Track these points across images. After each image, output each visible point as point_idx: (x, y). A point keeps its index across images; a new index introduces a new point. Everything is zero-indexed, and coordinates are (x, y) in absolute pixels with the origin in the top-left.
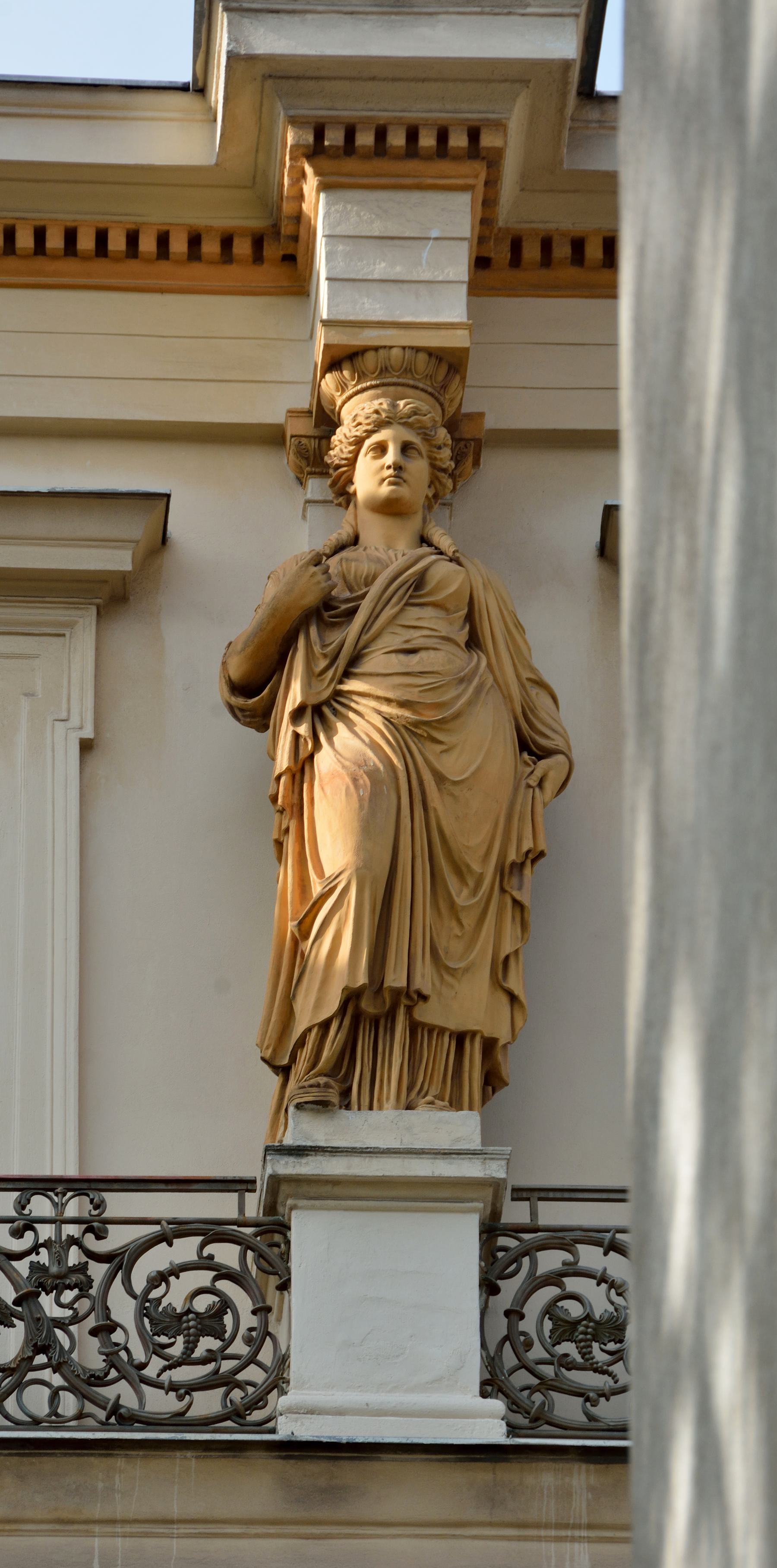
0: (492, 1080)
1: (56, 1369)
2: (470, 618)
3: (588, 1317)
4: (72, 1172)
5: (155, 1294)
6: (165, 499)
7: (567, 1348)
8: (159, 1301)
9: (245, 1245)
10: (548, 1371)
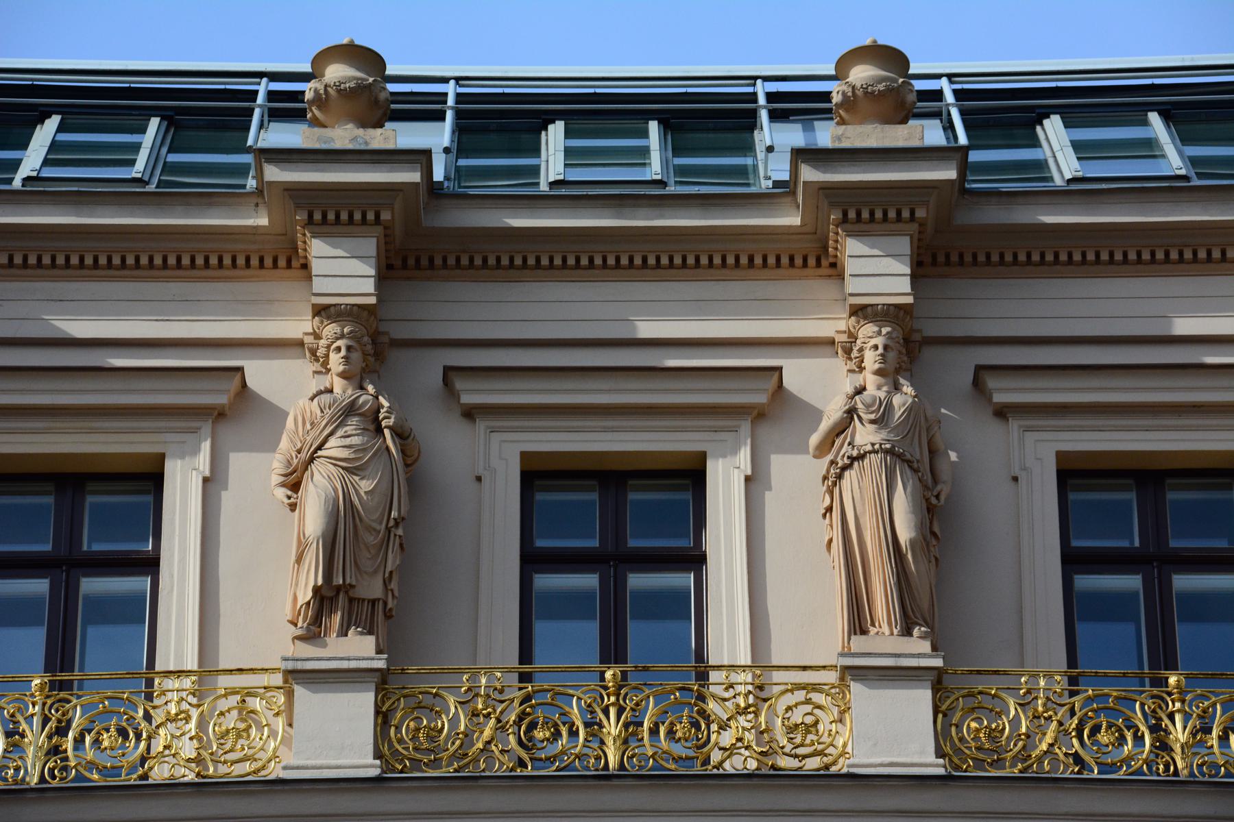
6: (451, 374)
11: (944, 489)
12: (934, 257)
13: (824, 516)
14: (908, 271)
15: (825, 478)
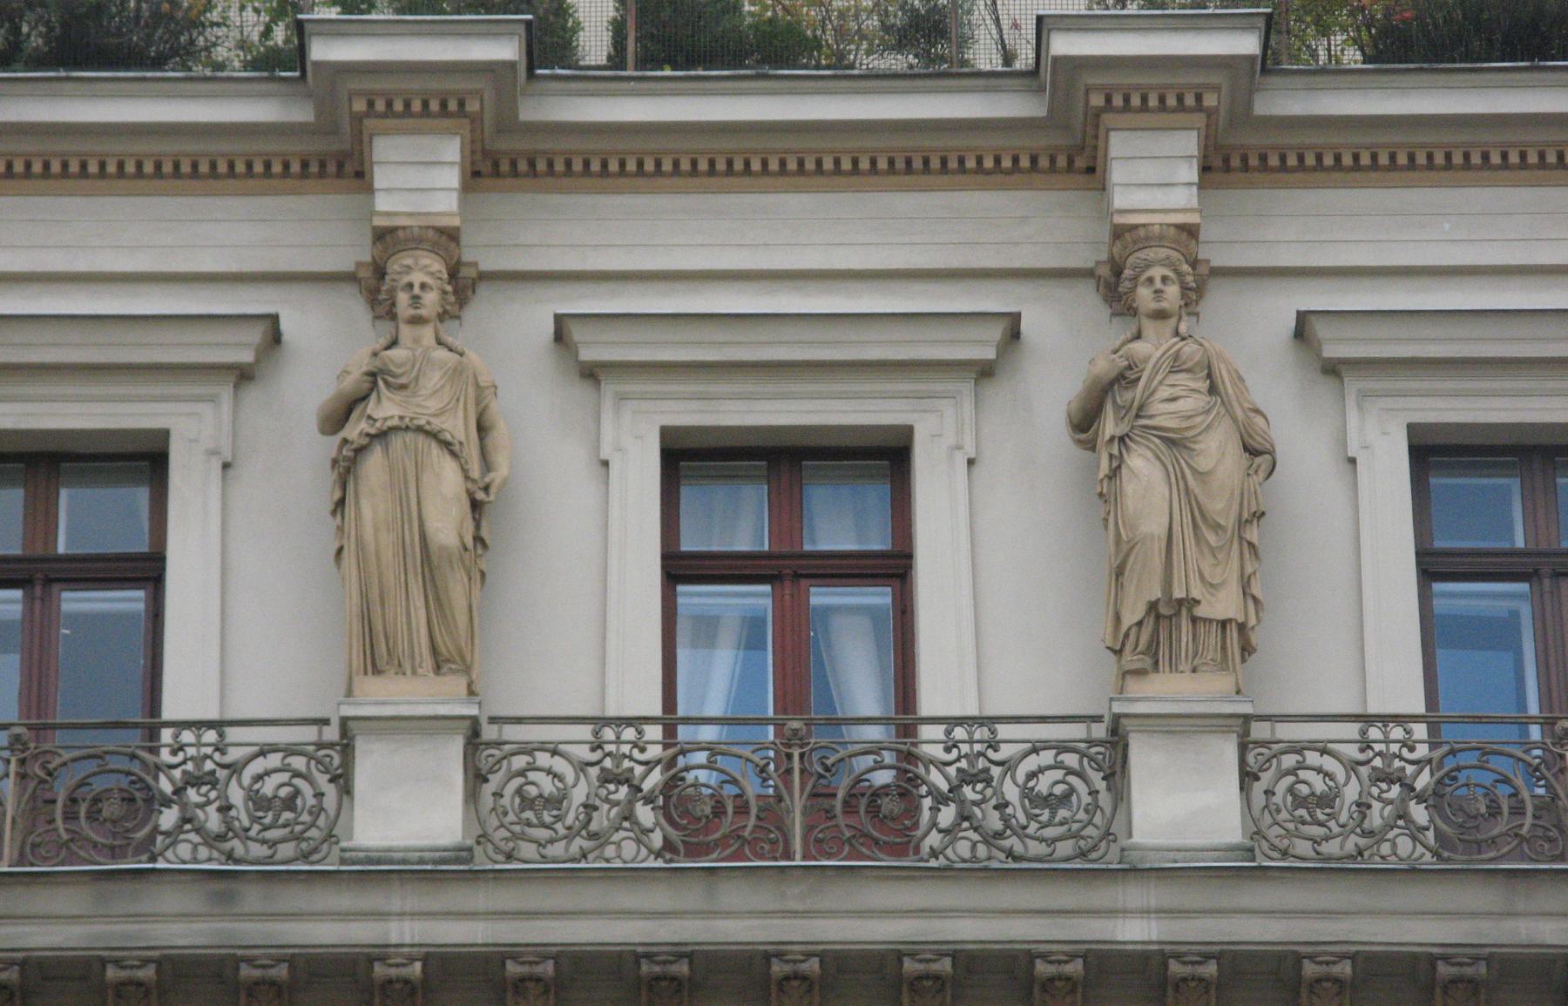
0: (1247, 649)
1: (976, 830)
2: (1209, 376)
3: (541, 796)
4: (975, 713)
5: (1031, 784)
7: (529, 814)
8: (1032, 789)
9: (310, 757)
10: (517, 828)
11: (497, 476)
12: (1226, 160)
13: (334, 513)
14: (1195, 179)
15: (335, 462)
